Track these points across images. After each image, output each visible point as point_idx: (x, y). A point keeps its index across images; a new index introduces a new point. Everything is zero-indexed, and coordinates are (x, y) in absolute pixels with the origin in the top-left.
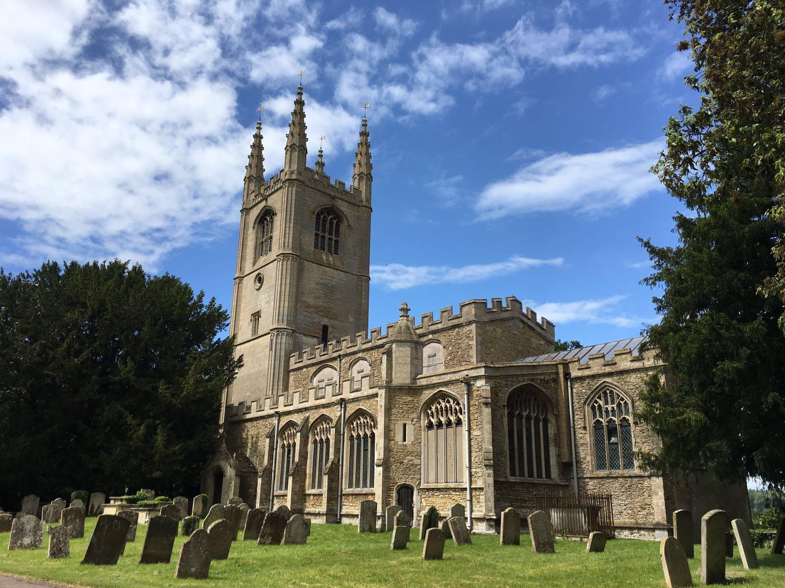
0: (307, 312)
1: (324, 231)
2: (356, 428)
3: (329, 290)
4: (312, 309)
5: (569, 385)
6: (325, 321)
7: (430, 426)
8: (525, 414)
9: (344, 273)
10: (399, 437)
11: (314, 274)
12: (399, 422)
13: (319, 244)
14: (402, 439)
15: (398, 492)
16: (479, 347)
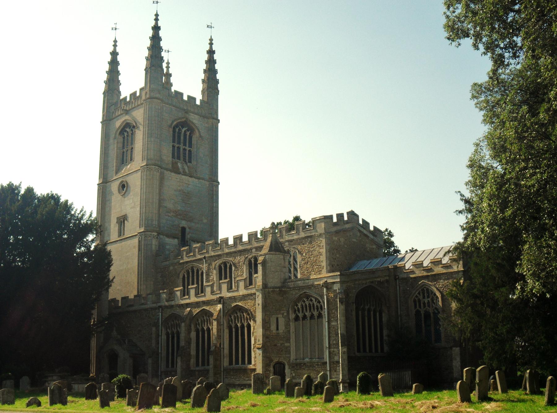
0: (169, 216)
1: (179, 143)
2: (233, 320)
3: (186, 196)
4: (172, 214)
5: (398, 284)
6: (184, 224)
7: (297, 319)
8: (367, 307)
9: (197, 180)
10: (273, 327)
11: (174, 182)
12: (273, 316)
13: (176, 154)
14: (276, 329)
15: (274, 367)
16: (328, 254)
